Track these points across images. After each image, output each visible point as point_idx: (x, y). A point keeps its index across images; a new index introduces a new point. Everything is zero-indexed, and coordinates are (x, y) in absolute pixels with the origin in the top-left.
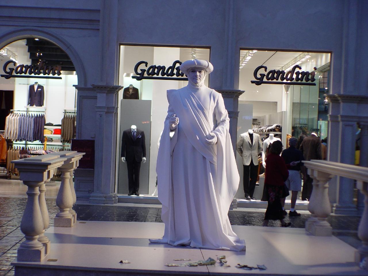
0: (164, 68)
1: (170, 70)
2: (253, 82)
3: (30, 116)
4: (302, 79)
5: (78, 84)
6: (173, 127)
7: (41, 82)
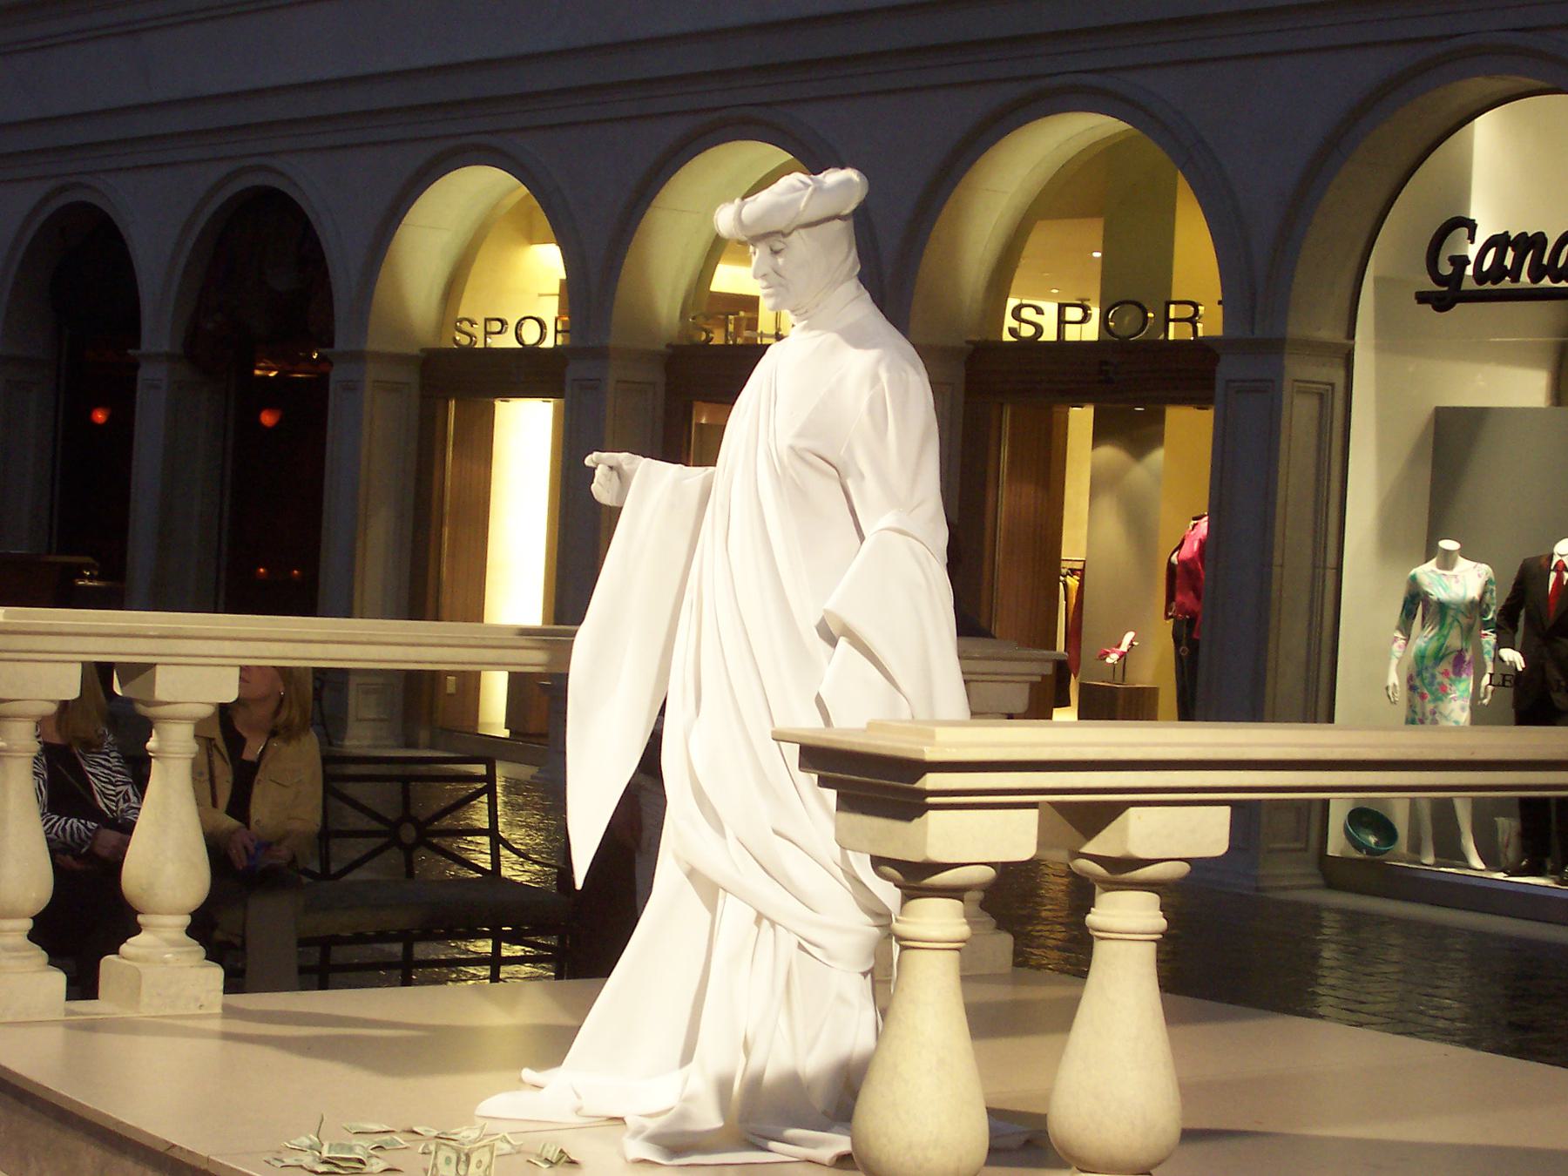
0: (1538, 241)
1: (1492, 253)
2: (1422, 298)
3: (33, 1159)
4: (1498, 271)
5: (1224, 329)
6: (785, 308)
7: (1346, 341)
